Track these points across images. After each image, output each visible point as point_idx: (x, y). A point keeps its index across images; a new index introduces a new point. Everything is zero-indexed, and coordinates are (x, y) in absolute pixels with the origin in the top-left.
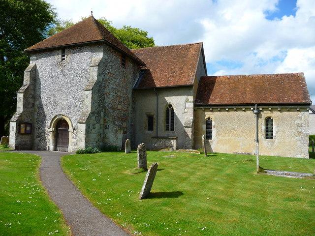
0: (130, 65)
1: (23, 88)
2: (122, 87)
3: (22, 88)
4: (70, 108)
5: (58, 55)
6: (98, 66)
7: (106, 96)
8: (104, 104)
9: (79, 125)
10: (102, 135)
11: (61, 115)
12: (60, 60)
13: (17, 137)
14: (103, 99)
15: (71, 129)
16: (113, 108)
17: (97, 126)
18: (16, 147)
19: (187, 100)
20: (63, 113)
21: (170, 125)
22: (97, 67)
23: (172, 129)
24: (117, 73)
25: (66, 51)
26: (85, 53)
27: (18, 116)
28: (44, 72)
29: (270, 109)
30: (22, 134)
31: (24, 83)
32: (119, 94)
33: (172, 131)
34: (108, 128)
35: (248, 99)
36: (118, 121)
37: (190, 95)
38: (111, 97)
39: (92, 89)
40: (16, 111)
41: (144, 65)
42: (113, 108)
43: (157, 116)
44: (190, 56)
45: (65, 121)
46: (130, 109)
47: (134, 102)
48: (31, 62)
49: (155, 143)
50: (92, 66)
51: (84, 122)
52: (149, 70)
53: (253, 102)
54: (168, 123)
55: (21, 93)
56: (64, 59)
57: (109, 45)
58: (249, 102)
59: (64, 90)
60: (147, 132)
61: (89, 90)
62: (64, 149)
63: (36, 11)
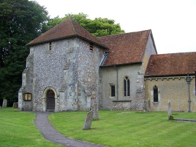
2: (91, 66)
4: (55, 82)
7: (78, 73)
8: (77, 78)
9: (60, 93)
10: (77, 100)
14: (77, 75)
15: (56, 97)
16: (84, 81)
17: (73, 94)
20: (51, 85)
23: (129, 95)
24: (87, 56)
25: (52, 43)
32: (88, 71)
35: (183, 71)
36: (88, 90)
38: (82, 73)
42: (84, 81)
43: (118, 86)
44: (141, 40)
46: (97, 81)
47: (101, 76)
49: (115, 105)
50: (69, 53)
53: (186, 73)
54: (125, 90)
55: (25, 73)
56: (51, 49)
57: (80, 38)
58: (183, 73)
59: (51, 70)
60: (111, 97)
62: (52, 110)
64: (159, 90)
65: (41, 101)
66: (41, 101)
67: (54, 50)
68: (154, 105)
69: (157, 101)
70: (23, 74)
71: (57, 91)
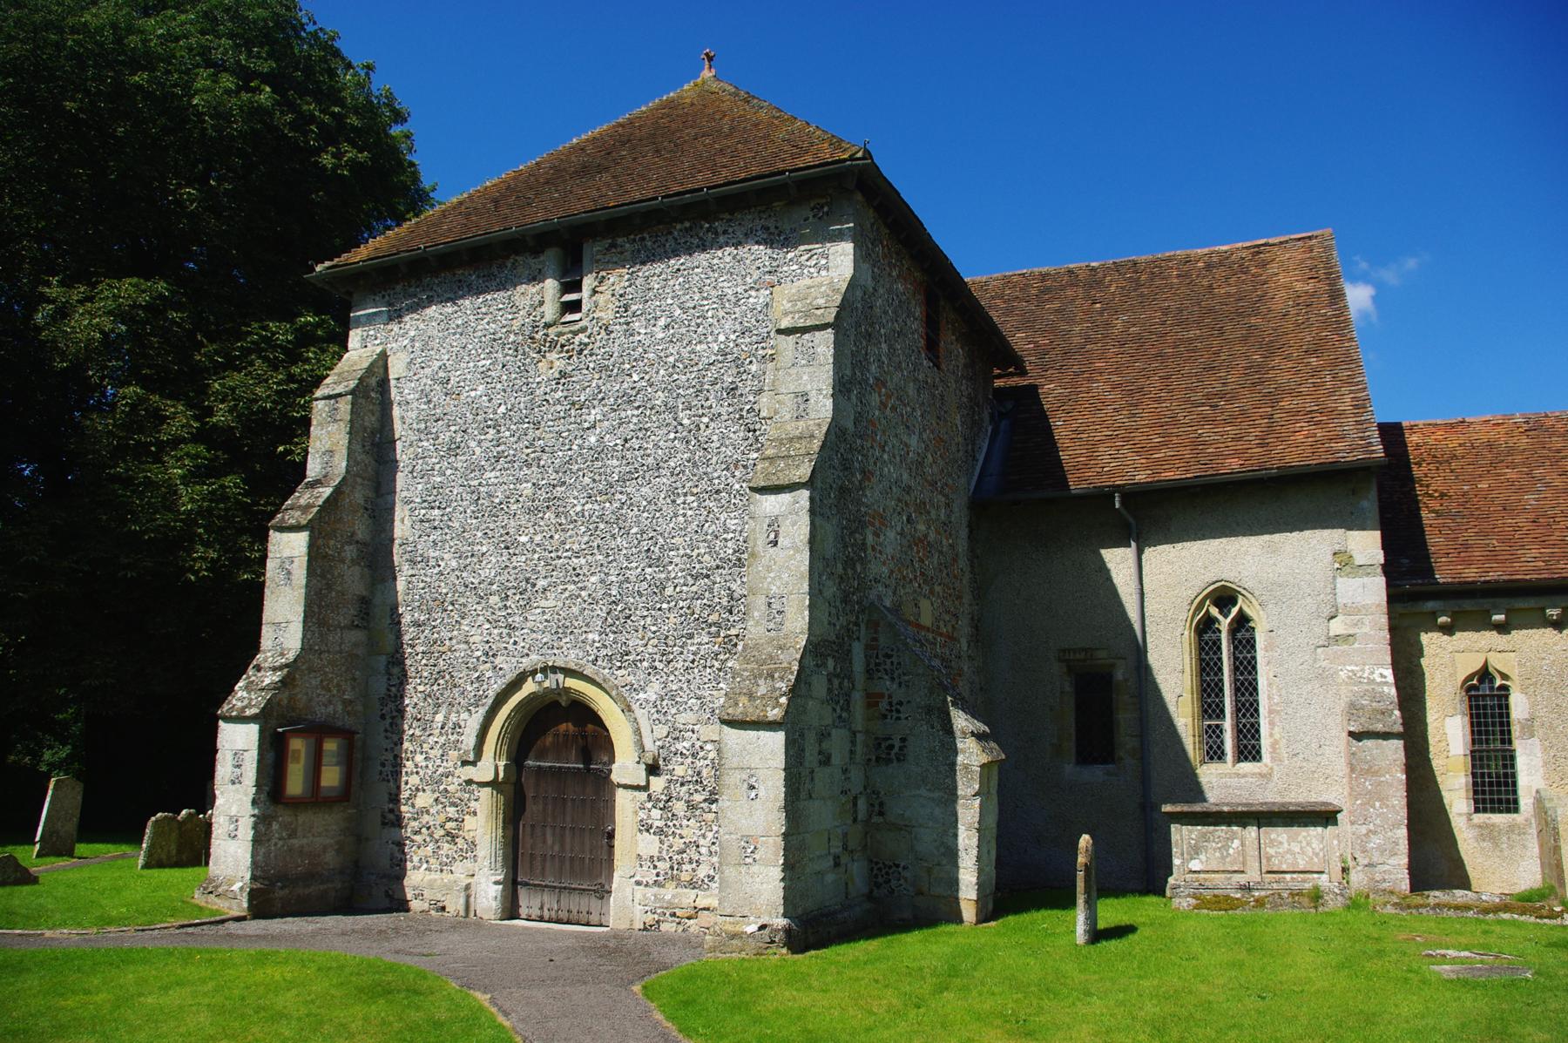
0: (955, 351)
1: (308, 499)
3: (302, 497)
4: (619, 619)
5: (536, 277)
6: (836, 325)
9: (733, 736)
11: (554, 669)
12: (550, 311)
13: (262, 825)
15: (625, 767)
18: (253, 895)
19: (1343, 561)
20: (570, 658)
21: (1228, 724)
22: (829, 334)
25: (591, 249)
26: (724, 256)
27: (269, 678)
28: (438, 395)
29: (1443, 619)
30: (297, 804)
31: (313, 469)
33: (1247, 767)
34: (901, 758)
37: (1362, 527)
39: (809, 484)
40: (255, 647)
41: (1011, 360)
45: (584, 714)
48: (355, 338)
51: (774, 714)
52: (1033, 390)
56: (575, 306)
61: (792, 487)
62: (575, 903)
63: (334, 134)
64: (1519, 706)
65: (452, 811)
66: (452, 811)
67: (607, 316)
68: (1481, 838)
69: (1511, 806)
70: (274, 536)
71: (640, 713)
